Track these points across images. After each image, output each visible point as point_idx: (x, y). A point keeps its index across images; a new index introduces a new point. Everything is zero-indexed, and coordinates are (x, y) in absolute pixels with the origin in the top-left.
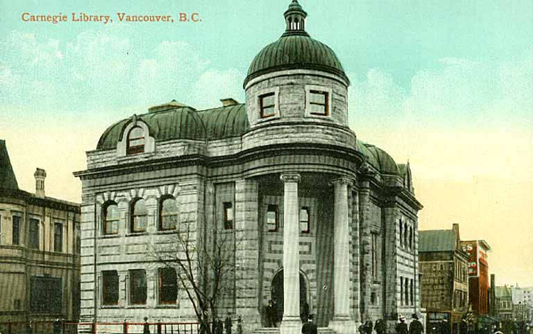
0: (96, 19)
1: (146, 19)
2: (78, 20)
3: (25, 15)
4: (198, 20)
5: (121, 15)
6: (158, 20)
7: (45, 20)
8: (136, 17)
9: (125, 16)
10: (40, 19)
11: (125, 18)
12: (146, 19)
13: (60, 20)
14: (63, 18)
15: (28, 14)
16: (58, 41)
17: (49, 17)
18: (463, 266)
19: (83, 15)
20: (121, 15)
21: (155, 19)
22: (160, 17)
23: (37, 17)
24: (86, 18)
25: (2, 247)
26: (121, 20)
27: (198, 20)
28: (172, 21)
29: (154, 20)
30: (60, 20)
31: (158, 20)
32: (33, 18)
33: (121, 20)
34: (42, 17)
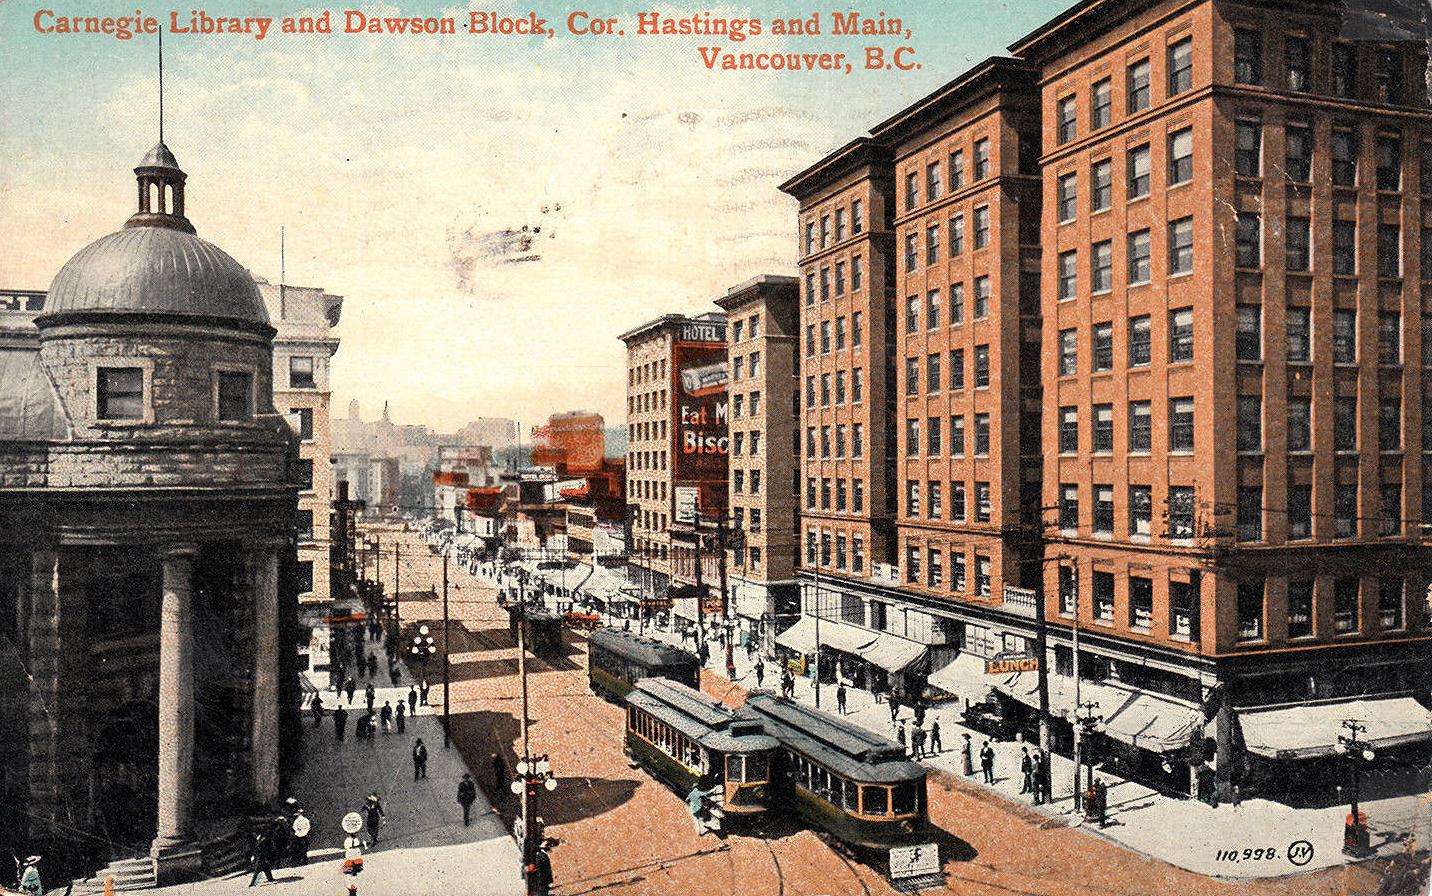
0: (236, 27)
1: (778, 61)
2: (186, 30)
3: (577, 19)
4: (911, 66)
5: (710, 54)
6: (810, 66)
7: (97, 30)
8: (724, 22)
9: (721, 55)
10: (82, 26)
11: (719, 60)
12: (778, 61)
13: (139, 30)
14: (146, 24)
15: (50, 13)
16: (371, 574)
17: (108, 21)
18: (670, 747)
19: (199, 18)
20: (710, 54)
21: (803, 63)
22: (816, 56)
23: (76, 21)
24: (207, 25)
25: (3, 336)
26: (709, 65)
27: (911, 66)
28: (849, 67)
29: (798, 67)
30: (139, 30)
31: (810, 66)
32: (63, 26)
33: (709, 65)
34: (88, 21)
